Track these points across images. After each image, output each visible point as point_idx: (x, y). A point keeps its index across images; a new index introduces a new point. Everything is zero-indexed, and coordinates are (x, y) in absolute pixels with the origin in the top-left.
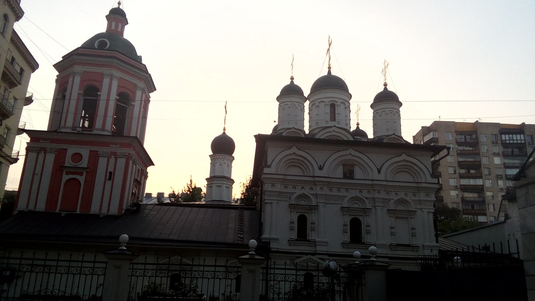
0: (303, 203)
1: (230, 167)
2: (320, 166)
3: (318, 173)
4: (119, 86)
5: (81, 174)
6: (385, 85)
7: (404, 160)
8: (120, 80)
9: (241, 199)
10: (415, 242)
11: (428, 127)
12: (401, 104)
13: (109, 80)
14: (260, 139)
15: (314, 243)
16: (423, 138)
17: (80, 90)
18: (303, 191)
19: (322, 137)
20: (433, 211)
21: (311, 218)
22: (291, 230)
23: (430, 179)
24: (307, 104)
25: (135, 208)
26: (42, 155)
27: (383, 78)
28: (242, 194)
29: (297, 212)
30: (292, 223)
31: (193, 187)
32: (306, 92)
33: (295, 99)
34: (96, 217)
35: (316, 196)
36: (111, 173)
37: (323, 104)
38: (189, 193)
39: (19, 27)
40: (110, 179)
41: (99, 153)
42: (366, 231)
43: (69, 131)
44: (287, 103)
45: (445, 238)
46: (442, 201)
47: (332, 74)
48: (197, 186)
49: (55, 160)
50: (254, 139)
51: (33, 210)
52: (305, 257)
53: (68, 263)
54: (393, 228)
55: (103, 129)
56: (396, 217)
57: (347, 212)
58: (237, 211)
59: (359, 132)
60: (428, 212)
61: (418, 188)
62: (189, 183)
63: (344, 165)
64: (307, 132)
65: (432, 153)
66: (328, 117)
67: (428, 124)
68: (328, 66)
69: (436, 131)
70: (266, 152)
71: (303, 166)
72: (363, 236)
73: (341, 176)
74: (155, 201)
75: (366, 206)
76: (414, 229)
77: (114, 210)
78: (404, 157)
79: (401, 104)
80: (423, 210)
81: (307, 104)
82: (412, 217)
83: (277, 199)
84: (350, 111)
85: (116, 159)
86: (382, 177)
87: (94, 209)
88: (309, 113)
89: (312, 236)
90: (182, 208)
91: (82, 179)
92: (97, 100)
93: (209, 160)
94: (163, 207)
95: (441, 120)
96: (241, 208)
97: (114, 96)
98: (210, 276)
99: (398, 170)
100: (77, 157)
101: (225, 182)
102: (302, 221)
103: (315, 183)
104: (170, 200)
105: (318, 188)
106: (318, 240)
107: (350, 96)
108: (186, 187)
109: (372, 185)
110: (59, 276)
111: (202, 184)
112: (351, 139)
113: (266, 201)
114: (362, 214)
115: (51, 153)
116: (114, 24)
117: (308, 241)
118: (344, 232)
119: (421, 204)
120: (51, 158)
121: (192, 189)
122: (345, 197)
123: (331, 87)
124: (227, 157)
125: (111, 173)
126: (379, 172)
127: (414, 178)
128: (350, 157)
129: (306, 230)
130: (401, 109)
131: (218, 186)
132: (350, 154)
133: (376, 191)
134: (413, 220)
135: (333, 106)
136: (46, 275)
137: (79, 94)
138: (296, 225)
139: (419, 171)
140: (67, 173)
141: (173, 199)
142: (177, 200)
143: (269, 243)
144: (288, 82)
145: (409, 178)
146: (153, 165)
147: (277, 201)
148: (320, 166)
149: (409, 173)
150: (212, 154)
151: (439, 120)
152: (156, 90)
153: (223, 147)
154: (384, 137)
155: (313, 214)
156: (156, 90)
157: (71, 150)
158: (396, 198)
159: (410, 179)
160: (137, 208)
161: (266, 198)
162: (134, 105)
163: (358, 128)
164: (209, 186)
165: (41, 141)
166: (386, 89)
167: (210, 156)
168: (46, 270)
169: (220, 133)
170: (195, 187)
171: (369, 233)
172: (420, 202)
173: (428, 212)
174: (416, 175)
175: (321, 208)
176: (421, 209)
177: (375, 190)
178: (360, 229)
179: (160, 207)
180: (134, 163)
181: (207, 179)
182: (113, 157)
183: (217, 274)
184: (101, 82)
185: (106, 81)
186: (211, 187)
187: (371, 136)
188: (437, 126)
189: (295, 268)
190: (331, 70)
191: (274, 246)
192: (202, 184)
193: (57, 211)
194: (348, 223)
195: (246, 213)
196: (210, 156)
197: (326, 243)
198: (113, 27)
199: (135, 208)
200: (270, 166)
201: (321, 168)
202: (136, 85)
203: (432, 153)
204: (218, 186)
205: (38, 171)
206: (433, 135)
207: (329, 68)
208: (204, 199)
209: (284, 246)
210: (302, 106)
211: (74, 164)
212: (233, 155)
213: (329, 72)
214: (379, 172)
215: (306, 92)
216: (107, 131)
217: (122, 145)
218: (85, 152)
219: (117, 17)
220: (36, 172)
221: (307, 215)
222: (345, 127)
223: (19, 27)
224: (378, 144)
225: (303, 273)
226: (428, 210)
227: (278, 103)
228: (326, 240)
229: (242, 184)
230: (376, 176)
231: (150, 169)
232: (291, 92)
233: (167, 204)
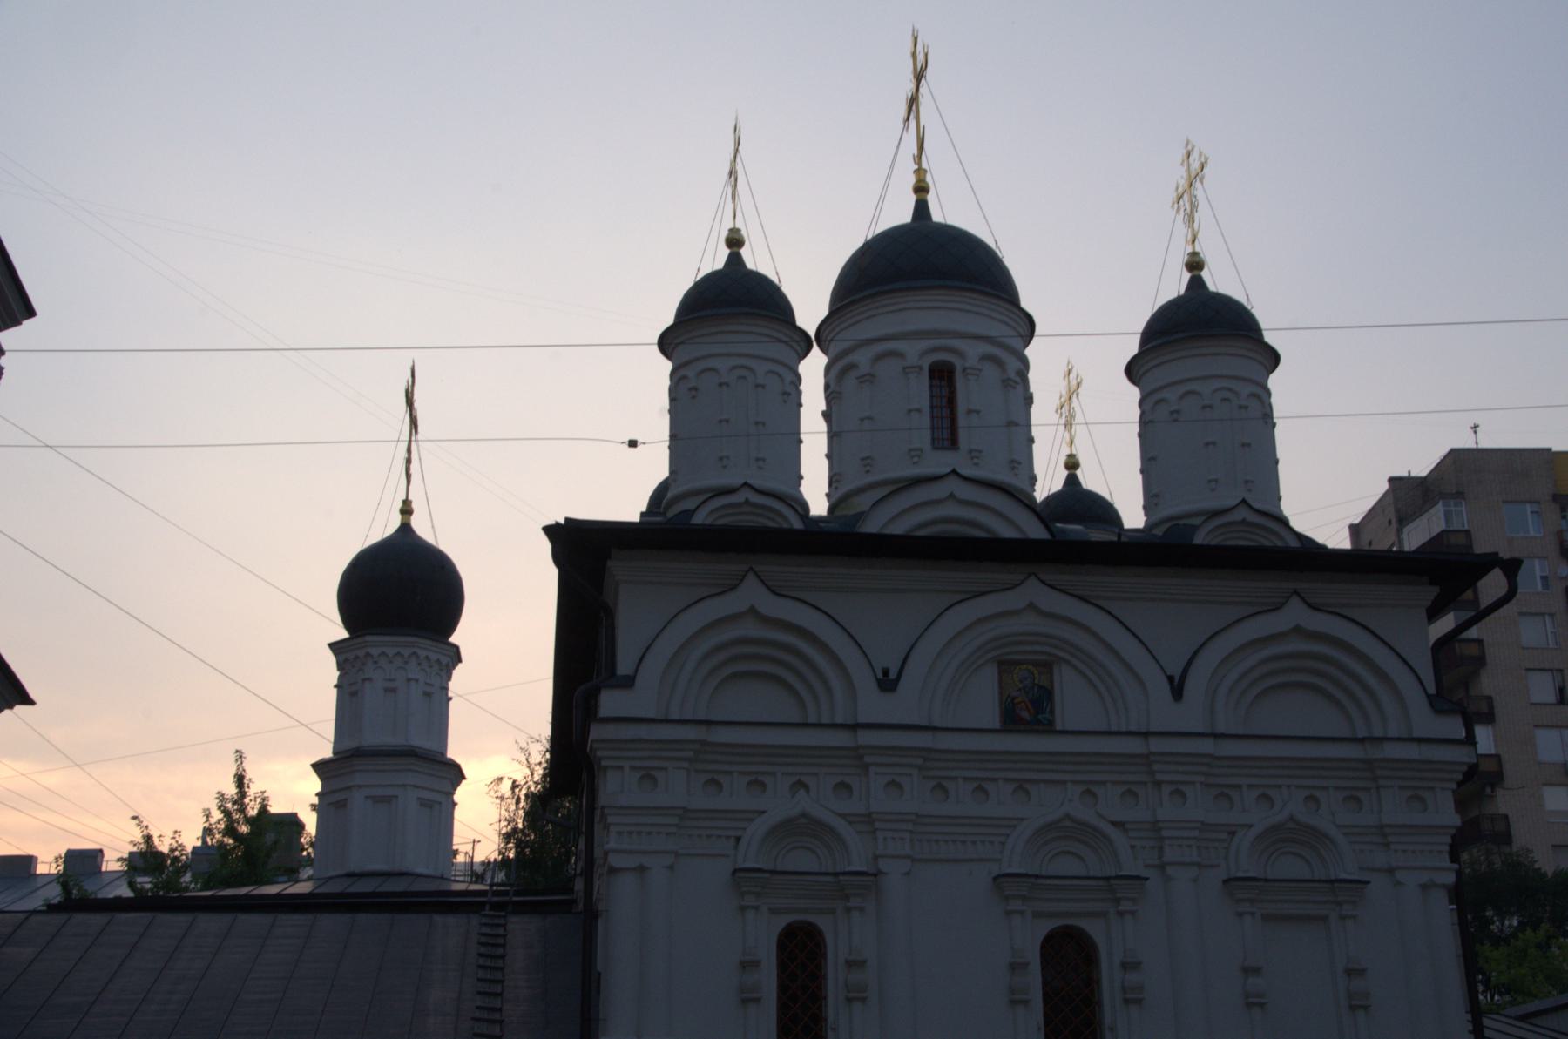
0: (801, 861)
1: (438, 702)
2: (886, 672)
3: (874, 706)
6: (1195, 264)
7: (1297, 630)
9: (504, 863)
11: (1421, 482)
12: (1272, 359)
14: (577, 546)
16: (1399, 531)
19: (898, 529)
20: (1451, 878)
21: (845, 937)
22: (745, 1001)
23: (1427, 723)
24: (813, 369)
27: (1182, 232)
28: (507, 837)
29: (773, 911)
30: (748, 965)
31: (253, 813)
32: (810, 311)
35: (868, 822)
38: (229, 841)
42: (1124, 989)
44: (711, 363)
45: (1524, 1018)
46: (1505, 837)
47: (937, 217)
48: (275, 808)
50: (546, 546)
54: (1256, 971)
56: (1267, 918)
58: (475, 920)
59: (1078, 502)
60: (1424, 887)
62: (231, 790)
63: (1005, 666)
64: (818, 505)
66: (923, 439)
67: (1421, 466)
68: (912, 180)
69: (1459, 495)
70: (610, 613)
71: (787, 666)
72: (1107, 1020)
73: (992, 718)
74: (54, 894)
76: (1361, 972)
78: (1295, 614)
79: (1272, 359)
81: (813, 369)
84: (1029, 400)
86: (1189, 715)
88: (826, 415)
90: (182, 919)
93: (328, 670)
94: (79, 917)
95: (1484, 444)
96: (496, 906)
102: (801, 952)
104: (131, 885)
107: (1028, 326)
108: (217, 815)
111: (293, 790)
112: (1036, 531)
113: (614, 860)
118: (1014, 1002)
119: (1387, 845)
121: (248, 820)
123: (929, 279)
124: (425, 648)
126: (1177, 690)
130: (1275, 381)
131: (377, 800)
132: (1032, 607)
133: (1166, 790)
135: (942, 375)
138: (768, 979)
139: (1371, 680)
141: (145, 882)
142: (172, 884)
144: (717, 259)
146: (27, 700)
148: (886, 672)
149: (1330, 697)
150: (343, 634)
151: (1470, 444)
152: (30, 312)
153: (400, 600)
154: (1196, 521)
156: (30, 312)
161: (612, 845)
163: (1072, 481)
164: (327, 804)
166: (1196, 284)
167: (335, 647)
169: (385, 526)
170: (263, 810)
171: (1139, 1002)
176: (1391, 871)
177: (1158, 784)
178: (1091, 984)
179: (58, 919)
181: (319, 767)
186: (341, 805)
187: (1133, 516)
188: (1464, 470)
190: (931, 199)
192: (293, 790)
195: (522, 929)
196: (335, 647)
200: (628, 682)
201: (887, 683)
203: (1434, 591)
204: (377, 800)
206: (1448, 515)
207: (921, 189)
208: (308, 872)
210: (789, 377)
212: (453, 639)
213: (921, 209)
214: (1177, 690)
215: (810, 311)
221: (823, 923)
222: (1003, 476)
224: (1165, 551)
227: (667, 366)
229: (505, 787)
230: (1165, 714)
232: (727, 313)
233: (118, 905)
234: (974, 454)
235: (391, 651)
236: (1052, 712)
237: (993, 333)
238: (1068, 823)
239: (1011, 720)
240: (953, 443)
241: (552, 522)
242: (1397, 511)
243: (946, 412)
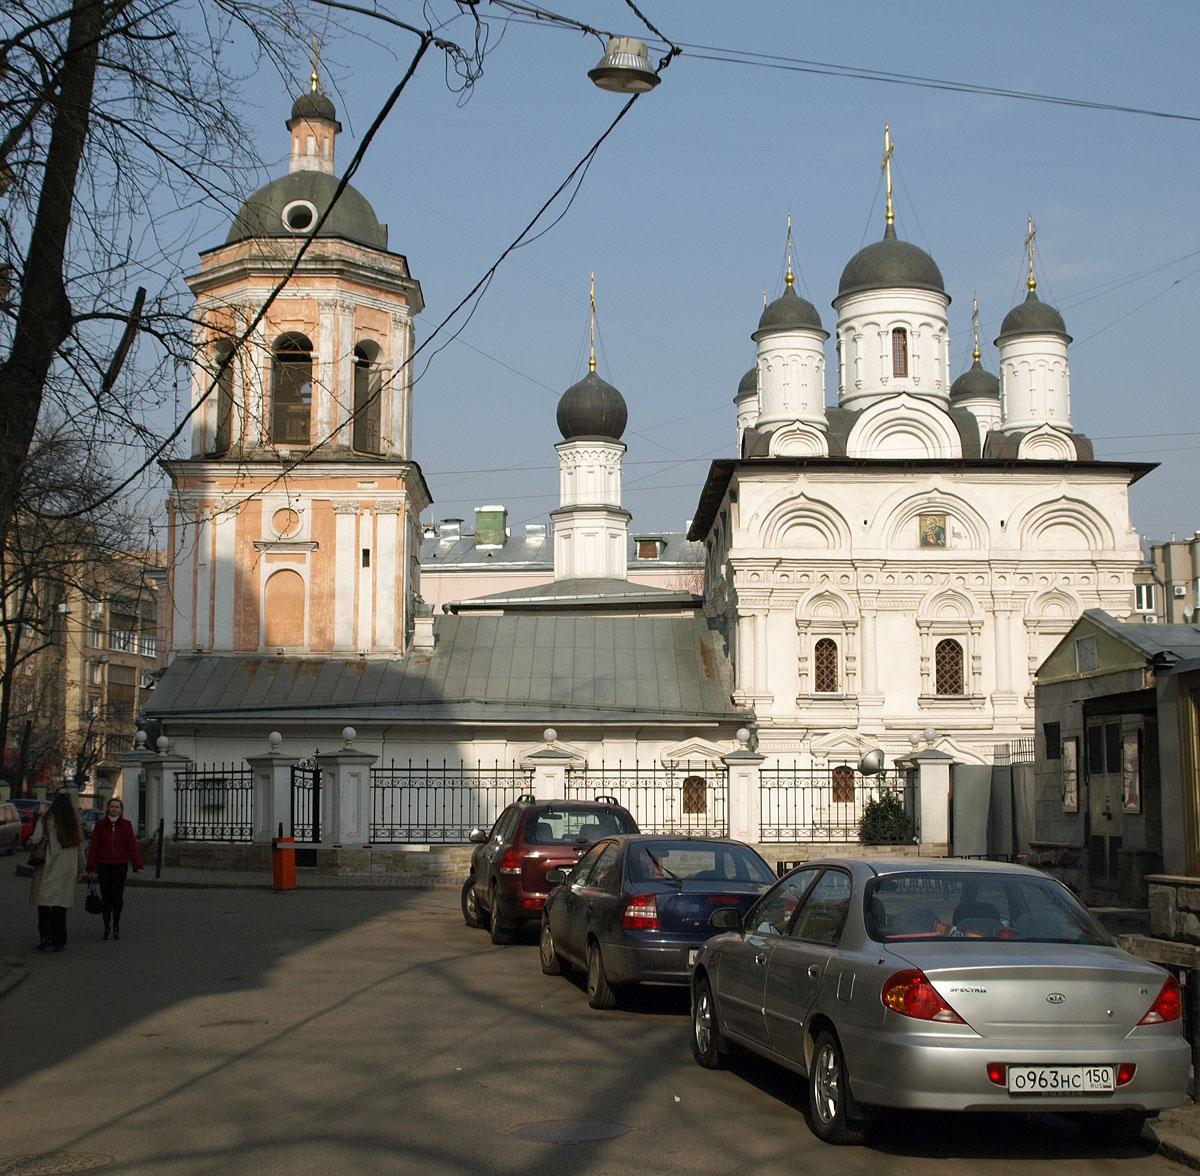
37: (873, 329)
53: (442, 772)
71: (1088, 527)
98: (664, 785)
110: (799, 791)
114: (964, 630)
115: (387, 513)
131: (587, 535)
135: (900, 333)
136: (642, 792)
158: (1041, 587)
168: (640, 785)
183: (499, 781)
204: (587, 535)
221: (836, 639)
234: (916, 380)
235: (590, 450)
236: (945, 539)
237: (914, 417)
238: (950, 592)
239: (925, 543)
240: (905, 374)
241: (594, 67)
242: (958, 764)
243: (902, 353)
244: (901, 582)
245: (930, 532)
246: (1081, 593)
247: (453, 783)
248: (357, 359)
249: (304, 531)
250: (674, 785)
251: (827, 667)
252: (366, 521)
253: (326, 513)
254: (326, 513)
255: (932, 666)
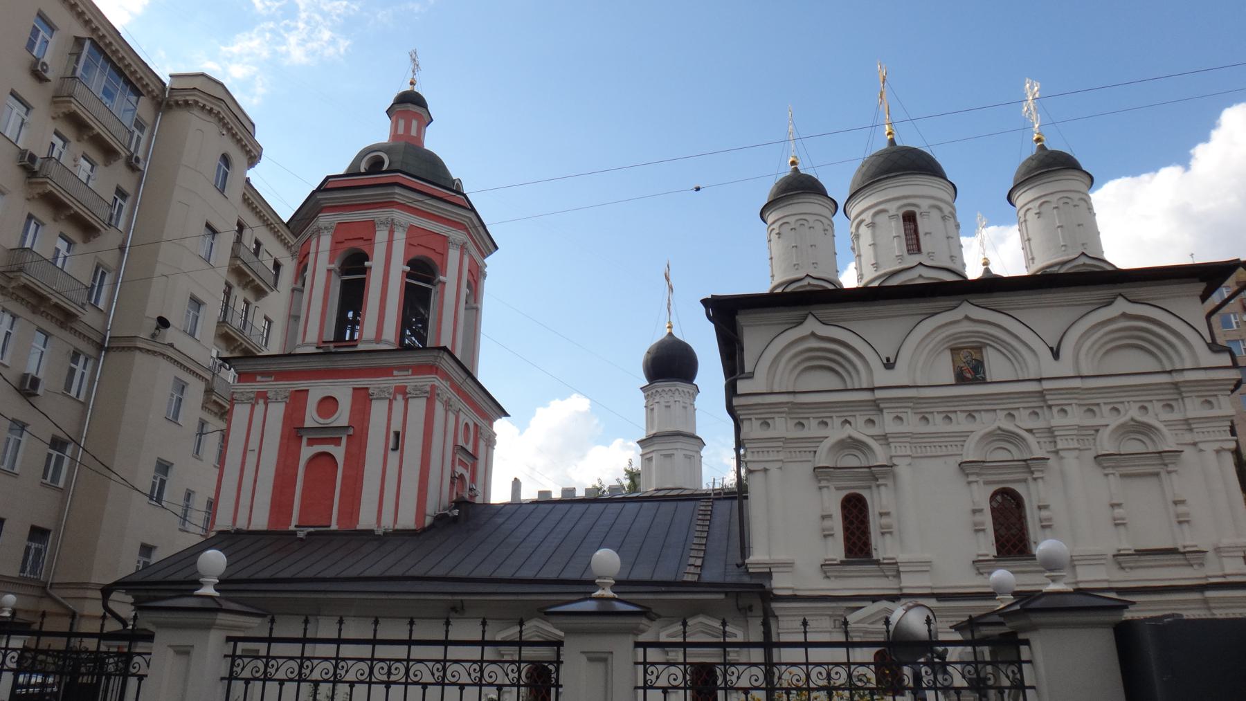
0: (851, 461)
2: (888, 359)
4: (409, 245)
5: (337, 441)
7: (1125, 316)
8: (412, 229)
10: (1185, 539)
13: (386, 233)
15: (894, 569)
17: (331, 261)
18: (848, 431)
21: (878, 501)
22: (825, 536)
25: (456, 512)
26: (260, 407)
29: (838, 489)
33: (808, 206)
34: (369, 533)
35: (884, 439)
36: (397, 434)
39: (256, 176)
40: (395, 449)
41: (371, 391)
43: (312, 350)
49: (287, 418)
51: (245, 528)
52: (870, 608)
55: (378, 339)
56: (1123, 476)
57: (977, 474)
60: (1218, 452)
61: (1176, 385)
63: (955, 351)
65: (1203, 286)
73: (951, 379)
75: (1031, 452)
77: (407, 520)
78: (1121, 306)
80: (1201, 446)
82: (1171, 468)
83: (781, 456)
85: (406, 400)
86: (1065, 366)
87: (366, 520)
89: (882, 548)
91: (339, 452)
92: (364, 279)
97: (399, 267)
99: (1114, 344)
100: (329, 403)
101: (678, 445)
102: (855, 509)
103: (876, 406)
105: (888, 417)
106: (901, 557)
109: (1041, 394)
116: (402, 123)
117: (877, 562)
119: (1191, 430)
120: (277, 411)
122: (966, 435)
125: (397, 434)
126: (1056, 354)
127: (1160, 361)
128: (966, 327)
129: (865, 532)
132: (967, 318)
133: (1055, 410)
134: (1174, 476)
136: (379, 690)
137: (329, 271)
140: (311, 442)
143: (769, 575)
145: (1149, 364)
147: (780, 464)
148: (888, 359)
155: (883, 488)
157: (317, 391)
158: (1114, 421)
159: (1152, 365)
160: (466, 515)
162: (444, 283)
165: (259, 378)
168: (379, 675)
171: (1049, 526)
172: (1188, 424)
173: (1218, 452)
174: (1159, 348)
175: (903, 469)
176: (1195, 444)
177: (1050, 407)
180: (447, 405)
182: (400, 397)
184: (371, 241)
185: (381, 236)
189: (842, 638)
191: (781, 583)
193: (292, 528)
194: (986, 506)
197: (925, 566)
198: (401, 131)
199: (456, 512)
200: (751, 376)
201: (889, 365)
202: (445, 239)
203: (1203, 286)
205: (254, 443)
209: (817, 584)
211: (321, 421)
214: (1056, 354)
215: (838, 188)
216: (387, 342)
217: (419, 369)
218: (343, 391)
219: (409, 106)
220: (250, 447)
221: (1020, 489)
223: (256, 176)
225: (867, 654)
226: (1217, 446)
228: (926, 556)
230: (1050, 367)
231: (499, 425)
239: (961, 379)
244: (938, 424)
245: (965, 367)
246: (1168, 423)
247: (389, 673)
248: (408, 269)
249: (342, 417)
250: (449, 678)
251: (858, 528)
252: (399, 404)
253: (362, 399)
254: (362, 399)
255: (987, 519)
